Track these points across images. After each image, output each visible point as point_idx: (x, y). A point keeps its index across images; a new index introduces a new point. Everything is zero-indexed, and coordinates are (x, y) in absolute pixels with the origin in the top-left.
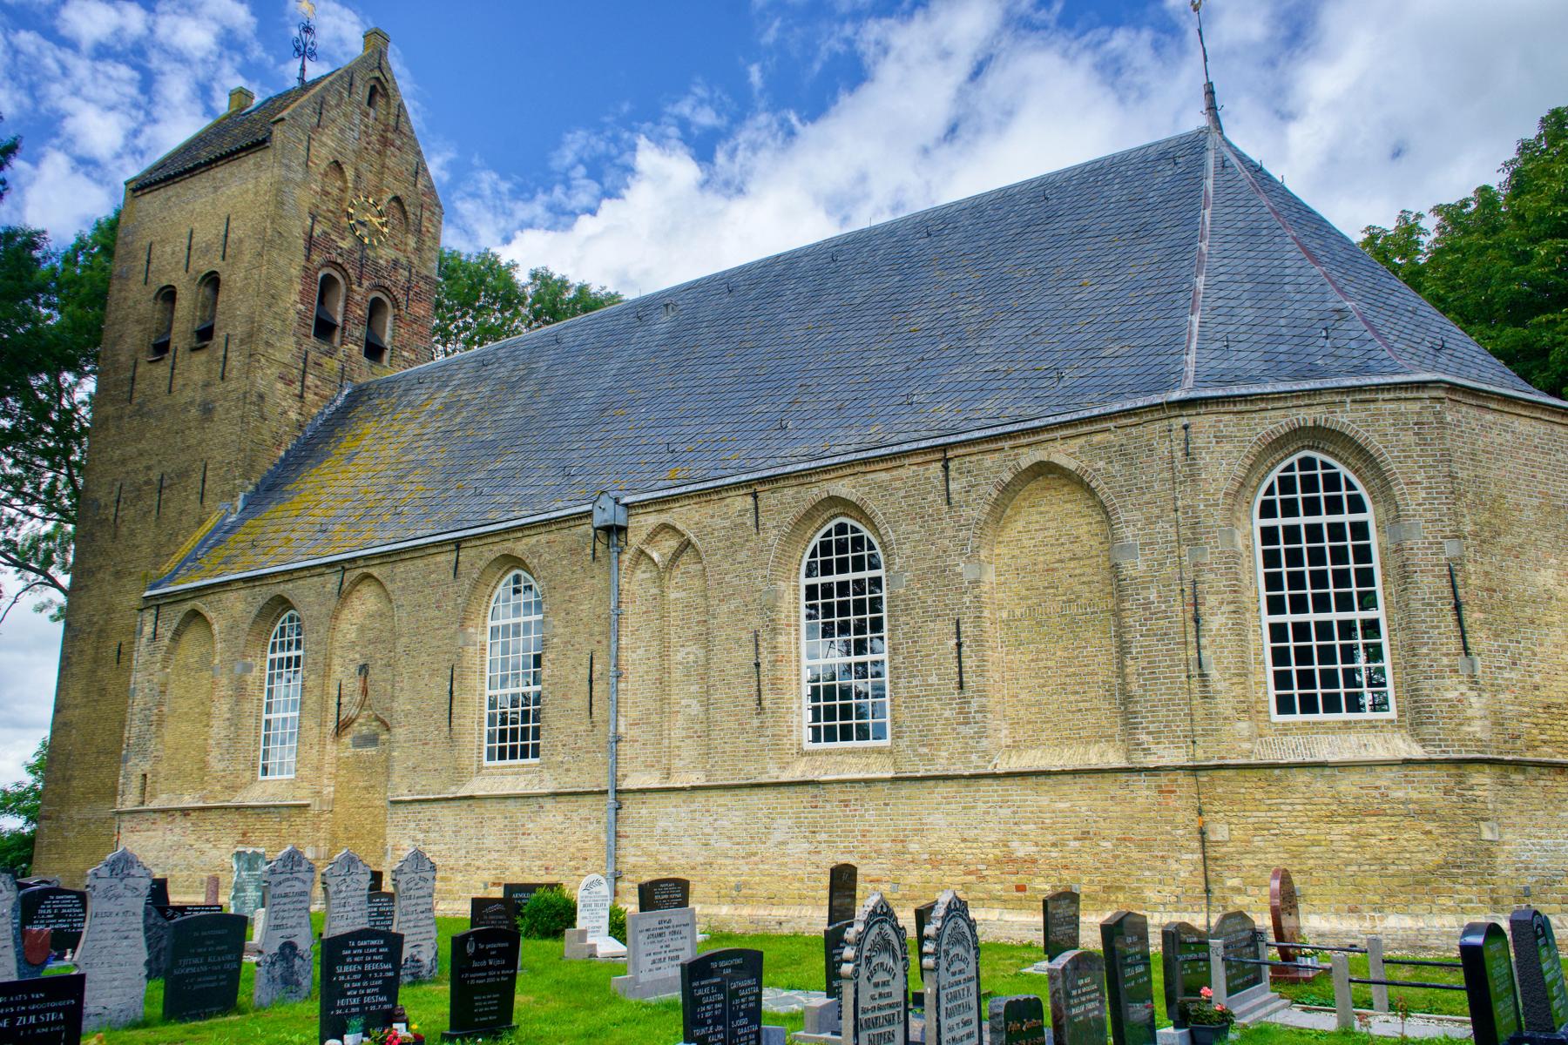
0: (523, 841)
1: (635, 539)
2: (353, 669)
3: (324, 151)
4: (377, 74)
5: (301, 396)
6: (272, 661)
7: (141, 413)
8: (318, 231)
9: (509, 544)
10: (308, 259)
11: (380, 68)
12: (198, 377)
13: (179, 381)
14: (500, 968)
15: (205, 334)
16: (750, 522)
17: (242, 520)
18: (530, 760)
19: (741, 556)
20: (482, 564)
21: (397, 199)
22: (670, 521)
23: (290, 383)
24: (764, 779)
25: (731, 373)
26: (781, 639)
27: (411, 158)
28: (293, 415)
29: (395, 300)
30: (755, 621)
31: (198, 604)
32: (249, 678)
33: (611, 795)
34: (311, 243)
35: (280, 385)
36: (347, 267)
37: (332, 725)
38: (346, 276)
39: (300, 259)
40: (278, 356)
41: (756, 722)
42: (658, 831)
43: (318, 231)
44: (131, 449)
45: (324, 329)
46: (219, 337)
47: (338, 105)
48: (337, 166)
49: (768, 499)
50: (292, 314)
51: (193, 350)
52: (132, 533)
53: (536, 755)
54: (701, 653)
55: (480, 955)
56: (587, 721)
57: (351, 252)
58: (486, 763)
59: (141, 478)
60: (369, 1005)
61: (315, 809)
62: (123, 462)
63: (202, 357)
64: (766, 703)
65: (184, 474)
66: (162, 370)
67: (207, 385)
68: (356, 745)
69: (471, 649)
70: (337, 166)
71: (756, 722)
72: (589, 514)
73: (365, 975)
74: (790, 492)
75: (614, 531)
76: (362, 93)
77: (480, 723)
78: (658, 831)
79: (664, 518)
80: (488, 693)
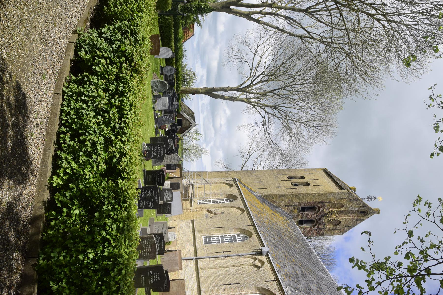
0: (185, 243)
1: (259, 257)
2: (223, 212)
3: (345, 202)
4: (369, 212)
5: (286, 206)
6: (218, 236)
7: (275, 177)
8: (326, 204)
9: (255, 234)
10: (318, 203)
11: (371, 213)
12: (286, 185)
13: (284, 182)
14: (157, 181)
15: (296, 185)
16: (267, 280)
17: (255, 195)
18: (204, 242)
19: (258, 279)
20: (249, 230)
21: (340, 222)
22: (265, 264)
23: (288, 202)
24: (201, 288)
25: (310, 284)
26: (238, 290)
27: (352, 225)
28: (281, 204)
29: (314, 226)
30: (242, 283)
31: (234, 185)
32: (219, 196)
33: (196, 258)
34: (322, 203)
35: (287, 200)
36: (320, 212)
37: (210, 209)
38: (318, 212)
39: (318, 200)
40: (294, 199)
41: (216, 285)
42: (188, 268)
43: (326, 204)
44: (267, 176)
45: (303, 209)
46: (296, 187)
47: (357, 204)
48: (343, 206)
49: (275, 283)
50: (304, 201)
51: (291, 183)
52: (249, 179)
53: (205, 243)
54: (232, 273)
55: (160, 175)
56: (214, 252)
57: (324, 212)
58: (203, 237)
59: (261, 179)
60: (150, 279)
61: (192, 208)
62: (264, 175)
63: (291, 185)
64: (221, 287)
65: (263, 185)
66: (286, 179)
67: (284, 186)
68: (206, 215)
69: (229, 231)
70: (343, 206)
71: (216, 285)
72: (264, 246)
73: (157, 151)
74: (277, 288)
75: (261, 253)
76: (363, 209)
77: (212, 235)
78: (188, 268)
79: (266, 263)
80: (219, 236)
